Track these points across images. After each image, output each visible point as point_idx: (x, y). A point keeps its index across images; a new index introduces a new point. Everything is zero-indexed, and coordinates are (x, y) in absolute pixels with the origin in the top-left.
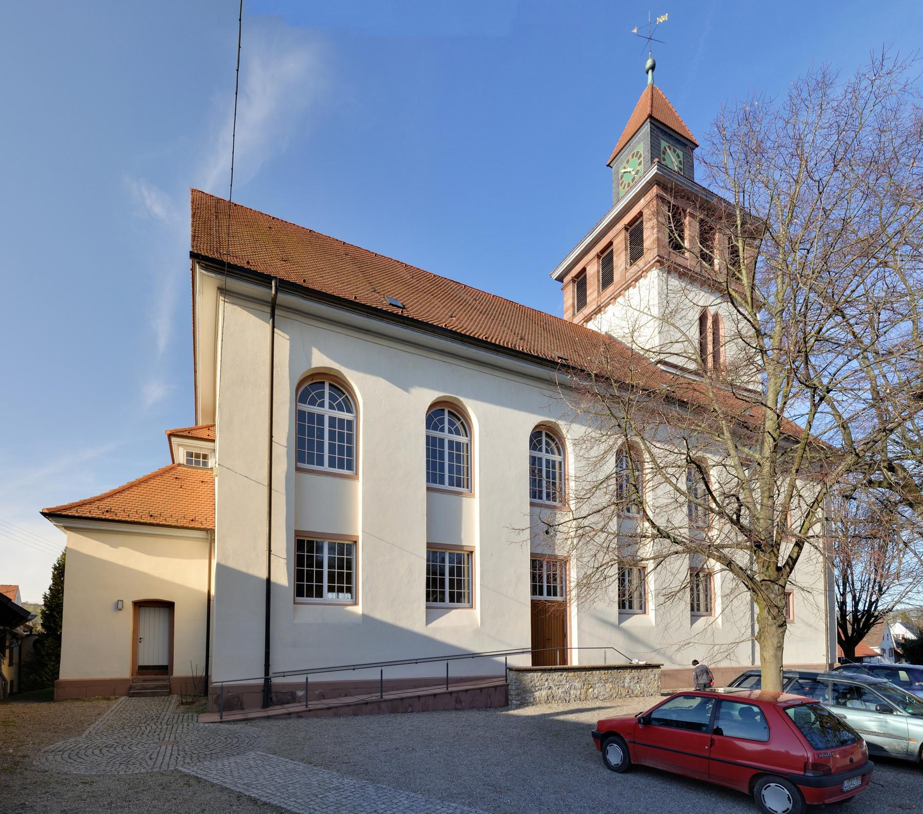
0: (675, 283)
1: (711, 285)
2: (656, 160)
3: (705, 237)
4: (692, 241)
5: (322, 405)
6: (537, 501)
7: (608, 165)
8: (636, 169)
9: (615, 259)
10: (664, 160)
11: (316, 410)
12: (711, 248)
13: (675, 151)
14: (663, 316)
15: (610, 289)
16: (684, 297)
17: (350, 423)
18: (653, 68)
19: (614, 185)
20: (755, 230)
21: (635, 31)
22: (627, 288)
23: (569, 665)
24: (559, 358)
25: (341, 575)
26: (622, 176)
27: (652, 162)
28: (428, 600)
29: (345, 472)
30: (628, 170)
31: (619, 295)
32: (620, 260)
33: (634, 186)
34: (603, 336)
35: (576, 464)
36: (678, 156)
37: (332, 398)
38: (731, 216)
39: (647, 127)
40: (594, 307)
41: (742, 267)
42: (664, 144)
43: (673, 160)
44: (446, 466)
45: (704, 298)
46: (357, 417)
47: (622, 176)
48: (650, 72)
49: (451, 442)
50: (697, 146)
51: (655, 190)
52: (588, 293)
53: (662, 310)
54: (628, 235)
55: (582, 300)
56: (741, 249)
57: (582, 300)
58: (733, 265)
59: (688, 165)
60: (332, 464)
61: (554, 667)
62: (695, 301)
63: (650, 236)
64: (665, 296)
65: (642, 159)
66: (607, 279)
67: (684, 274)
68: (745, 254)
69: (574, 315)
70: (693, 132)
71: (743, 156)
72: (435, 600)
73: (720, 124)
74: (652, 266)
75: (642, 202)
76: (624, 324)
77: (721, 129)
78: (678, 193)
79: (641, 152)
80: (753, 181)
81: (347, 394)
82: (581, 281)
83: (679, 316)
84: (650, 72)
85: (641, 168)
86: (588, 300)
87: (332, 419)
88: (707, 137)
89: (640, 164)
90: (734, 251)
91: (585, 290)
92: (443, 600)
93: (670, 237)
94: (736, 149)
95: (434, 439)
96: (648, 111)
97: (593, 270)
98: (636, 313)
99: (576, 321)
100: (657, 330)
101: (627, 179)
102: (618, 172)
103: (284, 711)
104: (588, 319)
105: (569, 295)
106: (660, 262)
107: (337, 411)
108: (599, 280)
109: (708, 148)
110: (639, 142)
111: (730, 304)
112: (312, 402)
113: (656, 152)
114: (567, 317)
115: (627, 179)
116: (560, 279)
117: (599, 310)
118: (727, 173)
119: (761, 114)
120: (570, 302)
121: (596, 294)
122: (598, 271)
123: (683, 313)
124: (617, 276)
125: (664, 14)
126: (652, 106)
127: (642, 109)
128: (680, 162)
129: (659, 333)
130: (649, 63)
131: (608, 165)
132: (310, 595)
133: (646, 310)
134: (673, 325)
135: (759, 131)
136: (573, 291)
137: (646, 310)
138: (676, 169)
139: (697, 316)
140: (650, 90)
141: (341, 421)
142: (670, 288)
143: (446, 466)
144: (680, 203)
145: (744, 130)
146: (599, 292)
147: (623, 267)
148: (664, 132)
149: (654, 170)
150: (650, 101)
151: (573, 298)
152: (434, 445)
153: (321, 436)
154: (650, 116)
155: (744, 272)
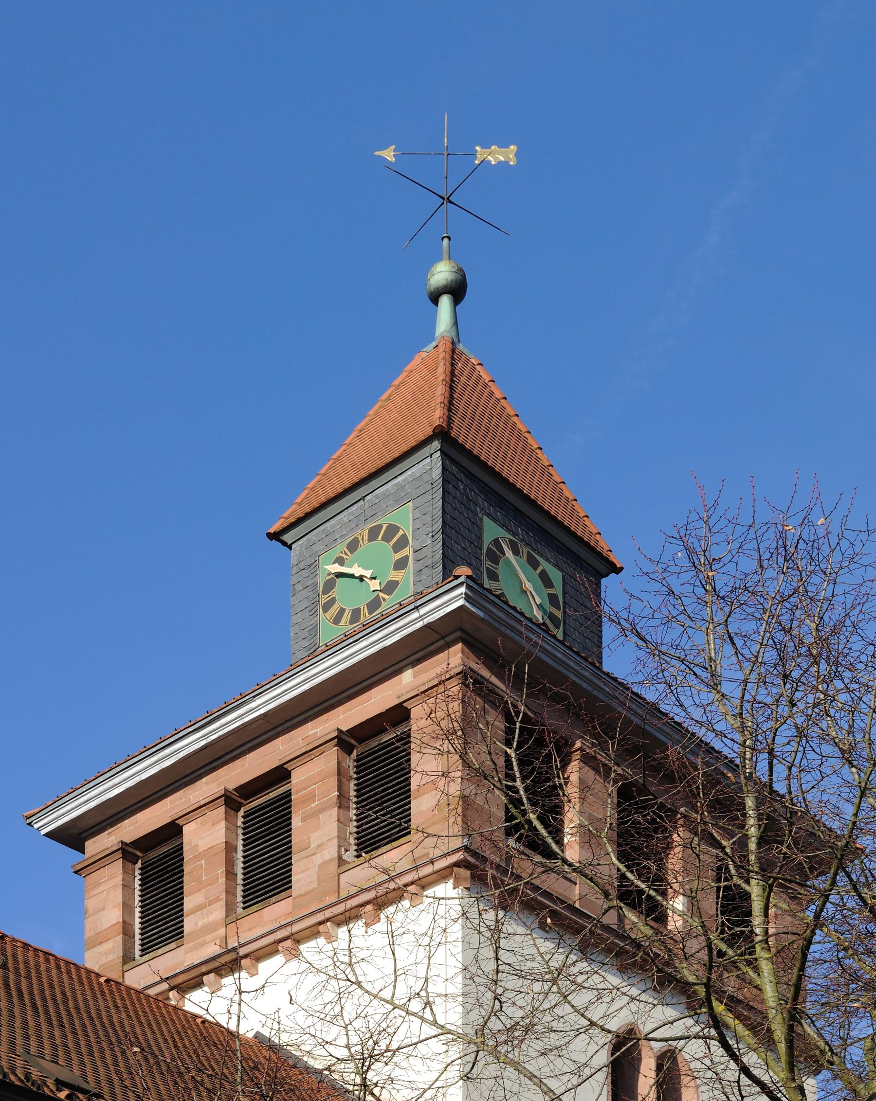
0: (529, 945)
1: (658, 972)
2: (464, 571)
3: (638, 839)
4: (588, 837)
7: (275, 536)
8: (384, 573)
9: (296, 822)
10: (494, 577)
12: (659, 880)
13: (534, 564)
14: (480, 1031)
15: (275, 913)
16: (553, 998)
18: (457, 291)
19: (300, 601)
20: (801, 852)
21: (389, 155)
22: (346, 919)
24: (61, 1084)
26: (329, 586)
27: (447, 573)
30: (357, 571)
31: (313, 933)
32: (319, 833)
33: (368, 629)
34: (245, 1043)
36: (546, 581)
38: (727, 807)
39: (430, 465)
40: (212, 950)
41: (760, 952)
42: (491, 531)
43: (527, 586)
45: (623, 1003)
47: (329, 586)
48: (445, 302)
50: (618, 570)
51: (455, 657)
52: (189, 903)
53: (476, 1017)
54: (350, 763)
55: (161, 916)
56: (757, 905)
57: (161, 916)
58: (731, 942)
59: (581, 613)
62: (595, 1015)
63: (435, 783)
64: (487, 983)
65: (407, 551)
66: (265, 871)
67: (558, 919)
68: (770, 916)
69: (127, 958)
70: (606, 526)
71: (770, 655)
73: (693, 542)
74: (441, 876)
75: (408, 681)
76: (332, 1032)
77: (700, 562)
78: (541, 680)
79: (407, 529)
80: (801, 733)
82: (159, 866)
83: (538, 1045)
84: (445, 302)
85: (406, 579)
86: (189, 924)
88: (648, 567)
89: (401, 564)
90: (735, 905)
91: (177, 896)
93: (509, 818)
94: (749, 626)
96: (437, 416)
97: (208, 839)
98: (377, 1010)
99: (138, 977)
100: (454, 1072)
101: (348, 597)
102: (313, 566)
103: (48, 997)
104: (190, 981)
105: (108, 900)
106: (475, 869)
108: (230, 874)
109: (656, 602)
110: (400, 502)
111: (715, 1045)
113: (458, 545)
114: (101, 958)
115: (348, 597)
116: (73, 836)
117: (229, 963)
118: (714, 686)
119: (837, 556)
120: (113, 916)
121: (218, 913)
122: (230, 848)
123: (554, 1039)
124: (305, 873)
125: (504, 145)
126: (450, 405)
127: (411, 400)
128: (553, 599)
129: (466, 1077)
130: (442, 273)
131: (275, 536)
133: (416, 1006)
134: (517, 1066)
135: (829, 600)
136: (127, 887)
137: (416, 1006)
138: (538, 615)
139: (603, 1057)
140: (442, 354)
142: (504, 956)
144: (554, 721)
145: (776, 583)
146: (230, 908)
147: (331, 852)
148: (485, 495)
149: (455, 599)
150: (441, 391)
151: (127, 907)
154: (442, 434)
155: (766, 967)
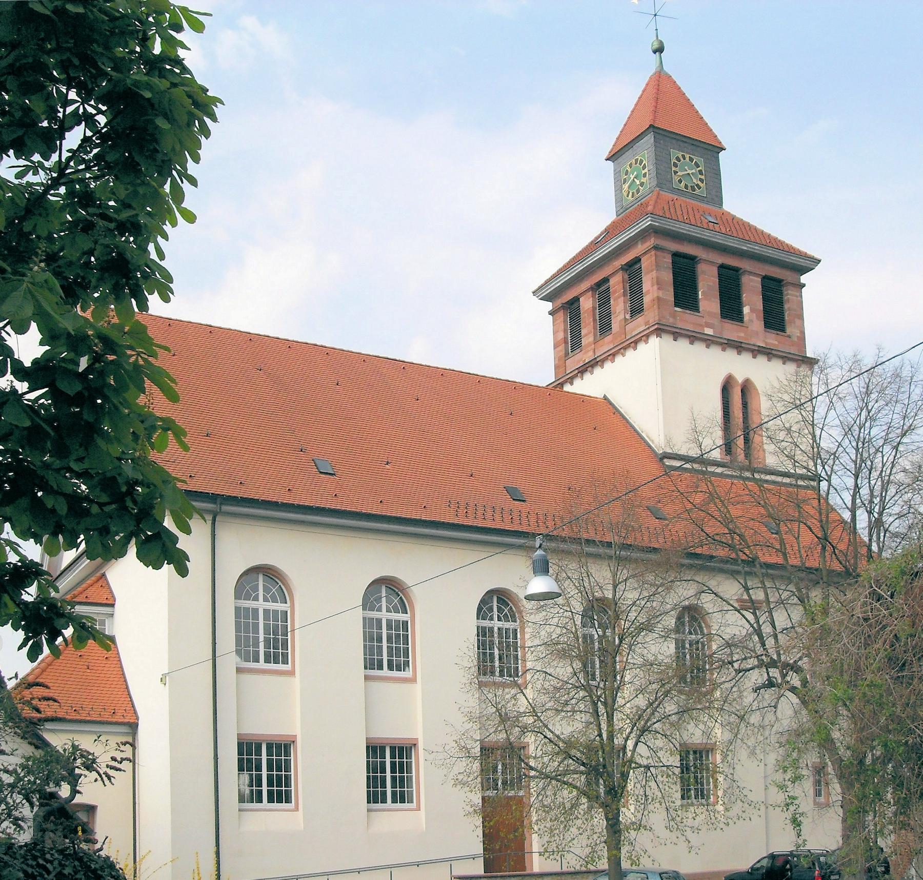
5: (256, 599)
6: (487, 679)
11: (394, 616)
17: (405, 624)
23: (528, 872)
25: (279, 778)
28: (369, 802)
29: (280, 667)
35: (537, 632)
37: (500, 610)
44: (388, 651)
46: (413, 617)
49: (266, 612)
60: (267, 661)
61: (515, 873)
72: (376, 802)
81: (280, 583)
87: (266, 612)
92: (384, 801)
95: (484, 628)
107: (393, 614)
112: (247, 598)
132: (280, 801)
141: (275, 612)
143: (388, 651)
152: (484, 635)
153: (256, 630)
